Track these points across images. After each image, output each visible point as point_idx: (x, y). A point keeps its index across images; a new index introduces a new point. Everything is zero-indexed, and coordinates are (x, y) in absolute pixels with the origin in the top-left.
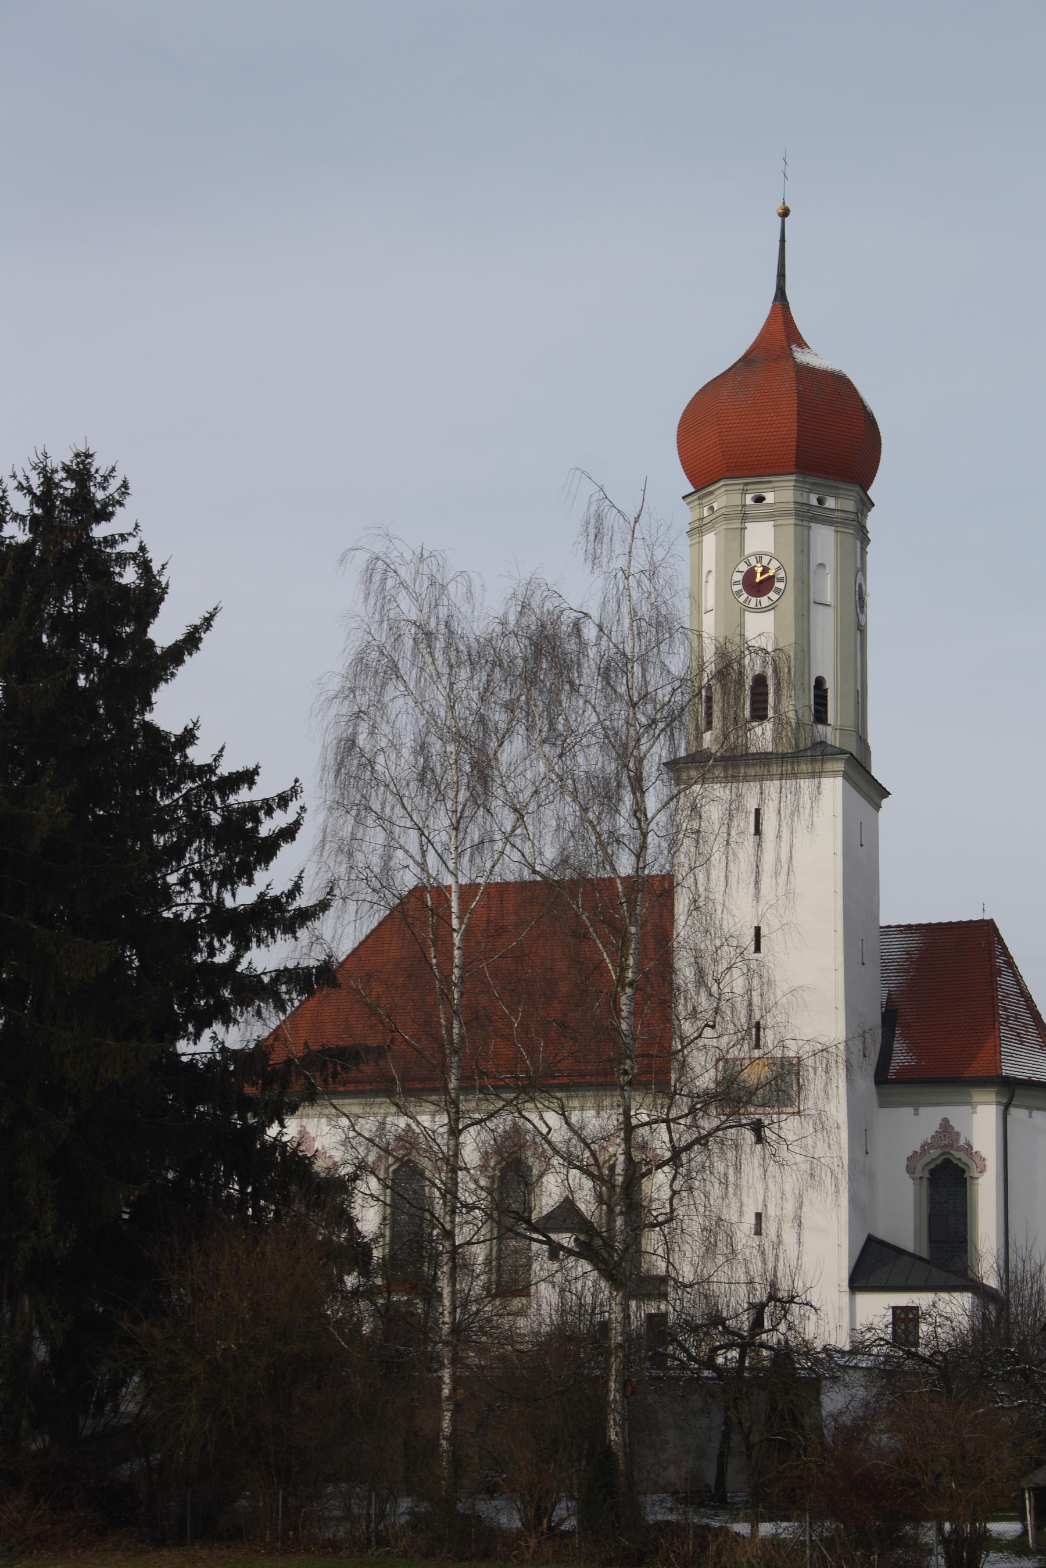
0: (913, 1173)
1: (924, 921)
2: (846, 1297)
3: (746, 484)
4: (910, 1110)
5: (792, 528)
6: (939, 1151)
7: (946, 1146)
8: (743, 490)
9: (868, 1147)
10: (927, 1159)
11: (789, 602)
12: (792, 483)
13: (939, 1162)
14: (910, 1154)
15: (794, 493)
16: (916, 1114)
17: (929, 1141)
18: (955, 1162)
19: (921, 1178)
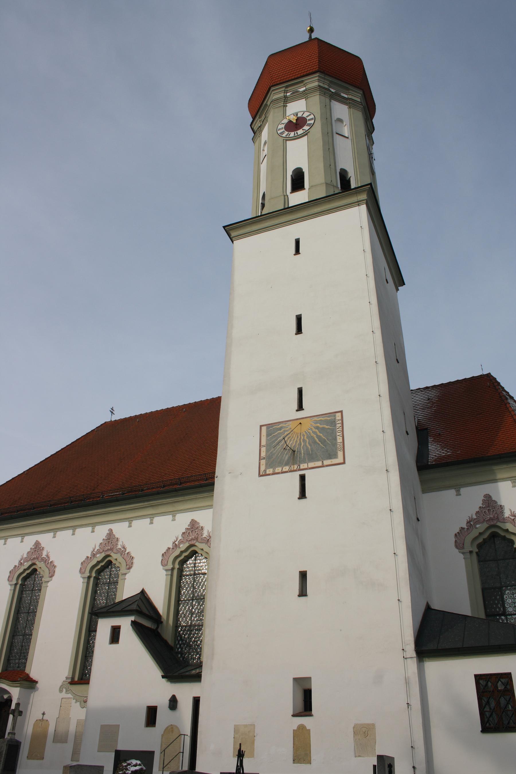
0: (463, 548)
1: (437, 383)
2: (413, 665)
3: (287, 87)
4: (452, 492)
5: (318, 96)
6: (485, 525)
7: (491, 519)
8: (285, 91)
9: (418, 515)
10: (474, 533)
11: (317, 131)
12: (319, 93)
13: (486, 536)
14: (458, 530)
15: (320, 98)
16: (458, 494)
17: (475, 517)
18: (502, 534)
19: (471, 552)
